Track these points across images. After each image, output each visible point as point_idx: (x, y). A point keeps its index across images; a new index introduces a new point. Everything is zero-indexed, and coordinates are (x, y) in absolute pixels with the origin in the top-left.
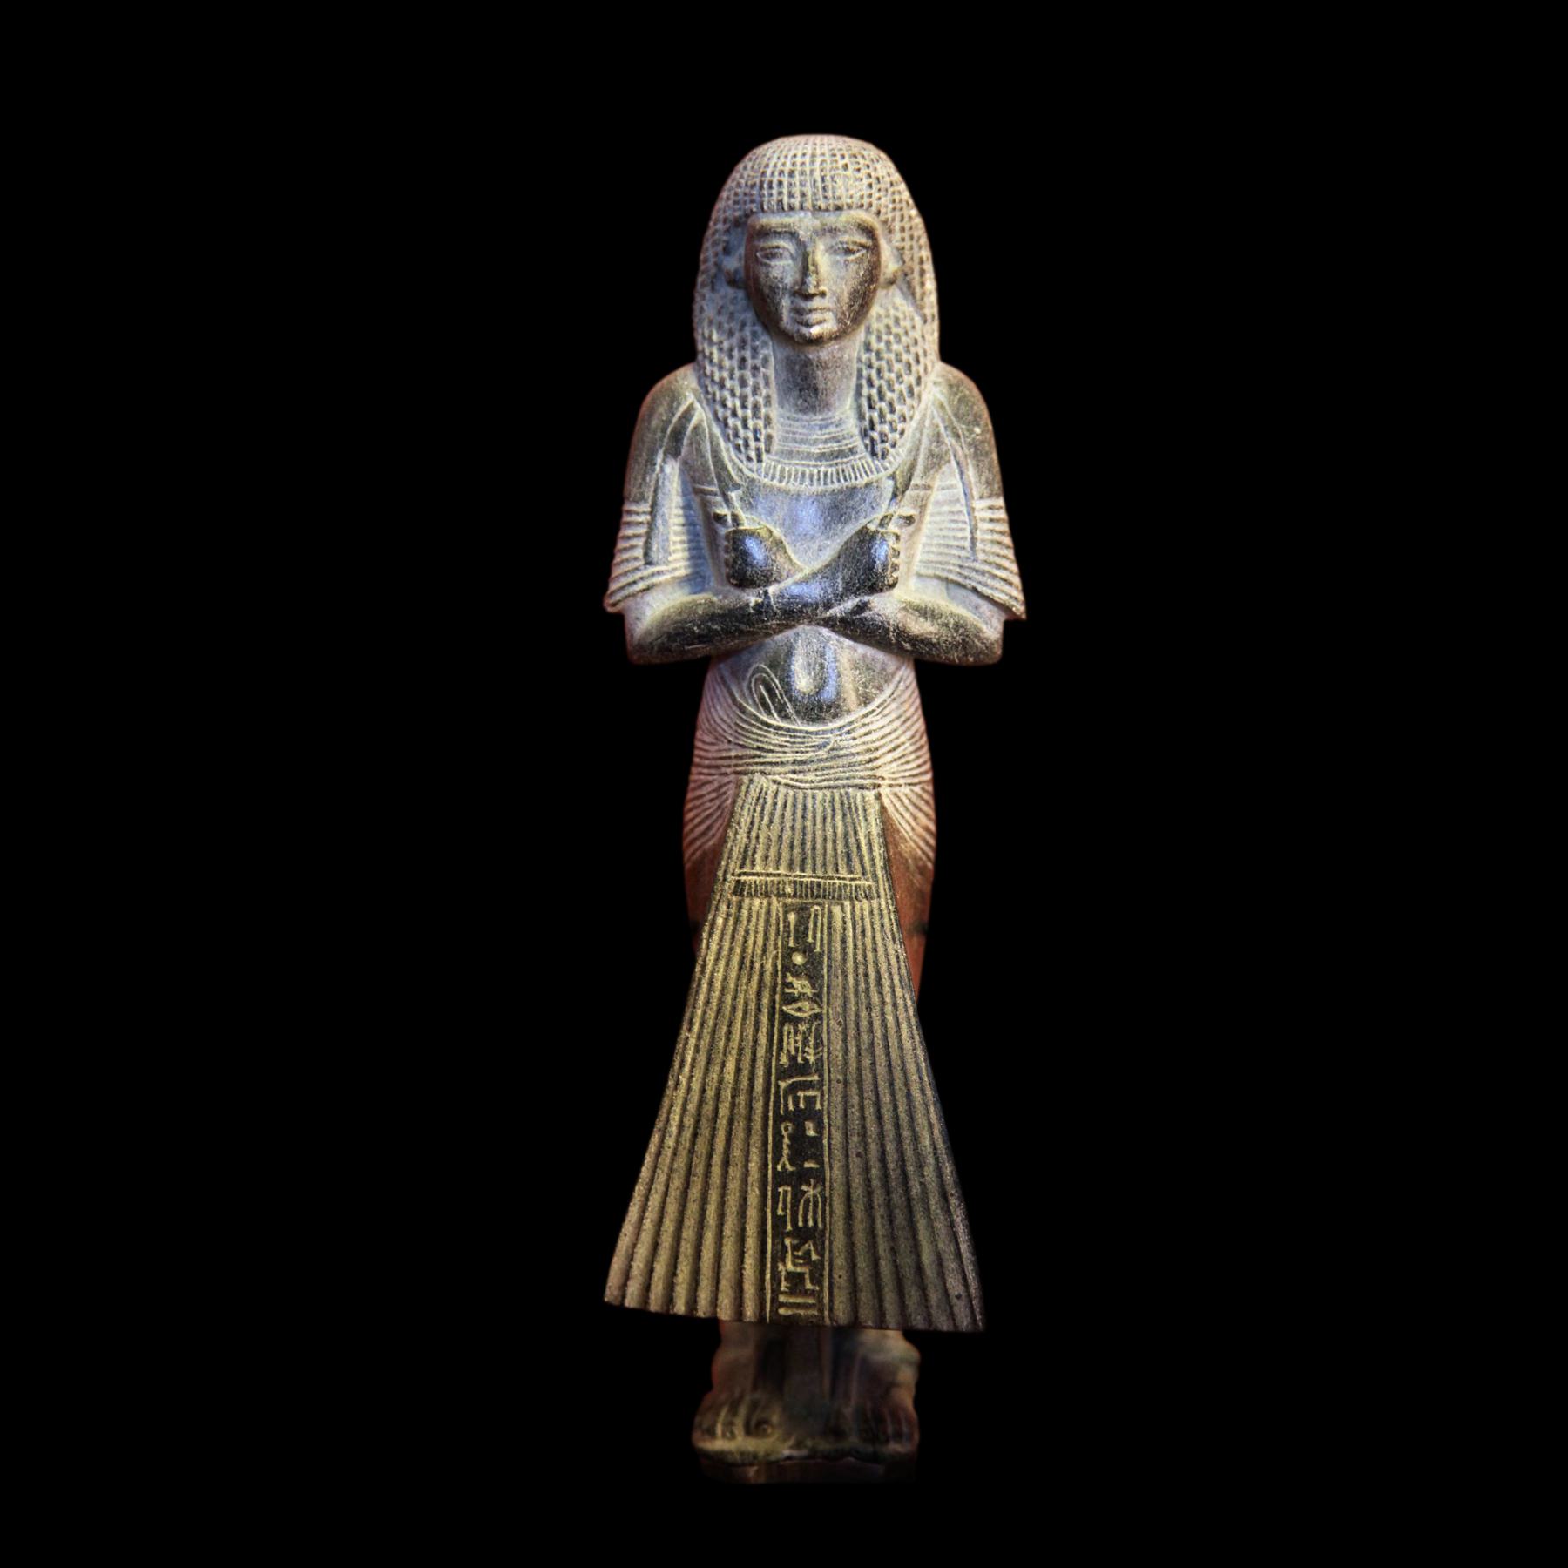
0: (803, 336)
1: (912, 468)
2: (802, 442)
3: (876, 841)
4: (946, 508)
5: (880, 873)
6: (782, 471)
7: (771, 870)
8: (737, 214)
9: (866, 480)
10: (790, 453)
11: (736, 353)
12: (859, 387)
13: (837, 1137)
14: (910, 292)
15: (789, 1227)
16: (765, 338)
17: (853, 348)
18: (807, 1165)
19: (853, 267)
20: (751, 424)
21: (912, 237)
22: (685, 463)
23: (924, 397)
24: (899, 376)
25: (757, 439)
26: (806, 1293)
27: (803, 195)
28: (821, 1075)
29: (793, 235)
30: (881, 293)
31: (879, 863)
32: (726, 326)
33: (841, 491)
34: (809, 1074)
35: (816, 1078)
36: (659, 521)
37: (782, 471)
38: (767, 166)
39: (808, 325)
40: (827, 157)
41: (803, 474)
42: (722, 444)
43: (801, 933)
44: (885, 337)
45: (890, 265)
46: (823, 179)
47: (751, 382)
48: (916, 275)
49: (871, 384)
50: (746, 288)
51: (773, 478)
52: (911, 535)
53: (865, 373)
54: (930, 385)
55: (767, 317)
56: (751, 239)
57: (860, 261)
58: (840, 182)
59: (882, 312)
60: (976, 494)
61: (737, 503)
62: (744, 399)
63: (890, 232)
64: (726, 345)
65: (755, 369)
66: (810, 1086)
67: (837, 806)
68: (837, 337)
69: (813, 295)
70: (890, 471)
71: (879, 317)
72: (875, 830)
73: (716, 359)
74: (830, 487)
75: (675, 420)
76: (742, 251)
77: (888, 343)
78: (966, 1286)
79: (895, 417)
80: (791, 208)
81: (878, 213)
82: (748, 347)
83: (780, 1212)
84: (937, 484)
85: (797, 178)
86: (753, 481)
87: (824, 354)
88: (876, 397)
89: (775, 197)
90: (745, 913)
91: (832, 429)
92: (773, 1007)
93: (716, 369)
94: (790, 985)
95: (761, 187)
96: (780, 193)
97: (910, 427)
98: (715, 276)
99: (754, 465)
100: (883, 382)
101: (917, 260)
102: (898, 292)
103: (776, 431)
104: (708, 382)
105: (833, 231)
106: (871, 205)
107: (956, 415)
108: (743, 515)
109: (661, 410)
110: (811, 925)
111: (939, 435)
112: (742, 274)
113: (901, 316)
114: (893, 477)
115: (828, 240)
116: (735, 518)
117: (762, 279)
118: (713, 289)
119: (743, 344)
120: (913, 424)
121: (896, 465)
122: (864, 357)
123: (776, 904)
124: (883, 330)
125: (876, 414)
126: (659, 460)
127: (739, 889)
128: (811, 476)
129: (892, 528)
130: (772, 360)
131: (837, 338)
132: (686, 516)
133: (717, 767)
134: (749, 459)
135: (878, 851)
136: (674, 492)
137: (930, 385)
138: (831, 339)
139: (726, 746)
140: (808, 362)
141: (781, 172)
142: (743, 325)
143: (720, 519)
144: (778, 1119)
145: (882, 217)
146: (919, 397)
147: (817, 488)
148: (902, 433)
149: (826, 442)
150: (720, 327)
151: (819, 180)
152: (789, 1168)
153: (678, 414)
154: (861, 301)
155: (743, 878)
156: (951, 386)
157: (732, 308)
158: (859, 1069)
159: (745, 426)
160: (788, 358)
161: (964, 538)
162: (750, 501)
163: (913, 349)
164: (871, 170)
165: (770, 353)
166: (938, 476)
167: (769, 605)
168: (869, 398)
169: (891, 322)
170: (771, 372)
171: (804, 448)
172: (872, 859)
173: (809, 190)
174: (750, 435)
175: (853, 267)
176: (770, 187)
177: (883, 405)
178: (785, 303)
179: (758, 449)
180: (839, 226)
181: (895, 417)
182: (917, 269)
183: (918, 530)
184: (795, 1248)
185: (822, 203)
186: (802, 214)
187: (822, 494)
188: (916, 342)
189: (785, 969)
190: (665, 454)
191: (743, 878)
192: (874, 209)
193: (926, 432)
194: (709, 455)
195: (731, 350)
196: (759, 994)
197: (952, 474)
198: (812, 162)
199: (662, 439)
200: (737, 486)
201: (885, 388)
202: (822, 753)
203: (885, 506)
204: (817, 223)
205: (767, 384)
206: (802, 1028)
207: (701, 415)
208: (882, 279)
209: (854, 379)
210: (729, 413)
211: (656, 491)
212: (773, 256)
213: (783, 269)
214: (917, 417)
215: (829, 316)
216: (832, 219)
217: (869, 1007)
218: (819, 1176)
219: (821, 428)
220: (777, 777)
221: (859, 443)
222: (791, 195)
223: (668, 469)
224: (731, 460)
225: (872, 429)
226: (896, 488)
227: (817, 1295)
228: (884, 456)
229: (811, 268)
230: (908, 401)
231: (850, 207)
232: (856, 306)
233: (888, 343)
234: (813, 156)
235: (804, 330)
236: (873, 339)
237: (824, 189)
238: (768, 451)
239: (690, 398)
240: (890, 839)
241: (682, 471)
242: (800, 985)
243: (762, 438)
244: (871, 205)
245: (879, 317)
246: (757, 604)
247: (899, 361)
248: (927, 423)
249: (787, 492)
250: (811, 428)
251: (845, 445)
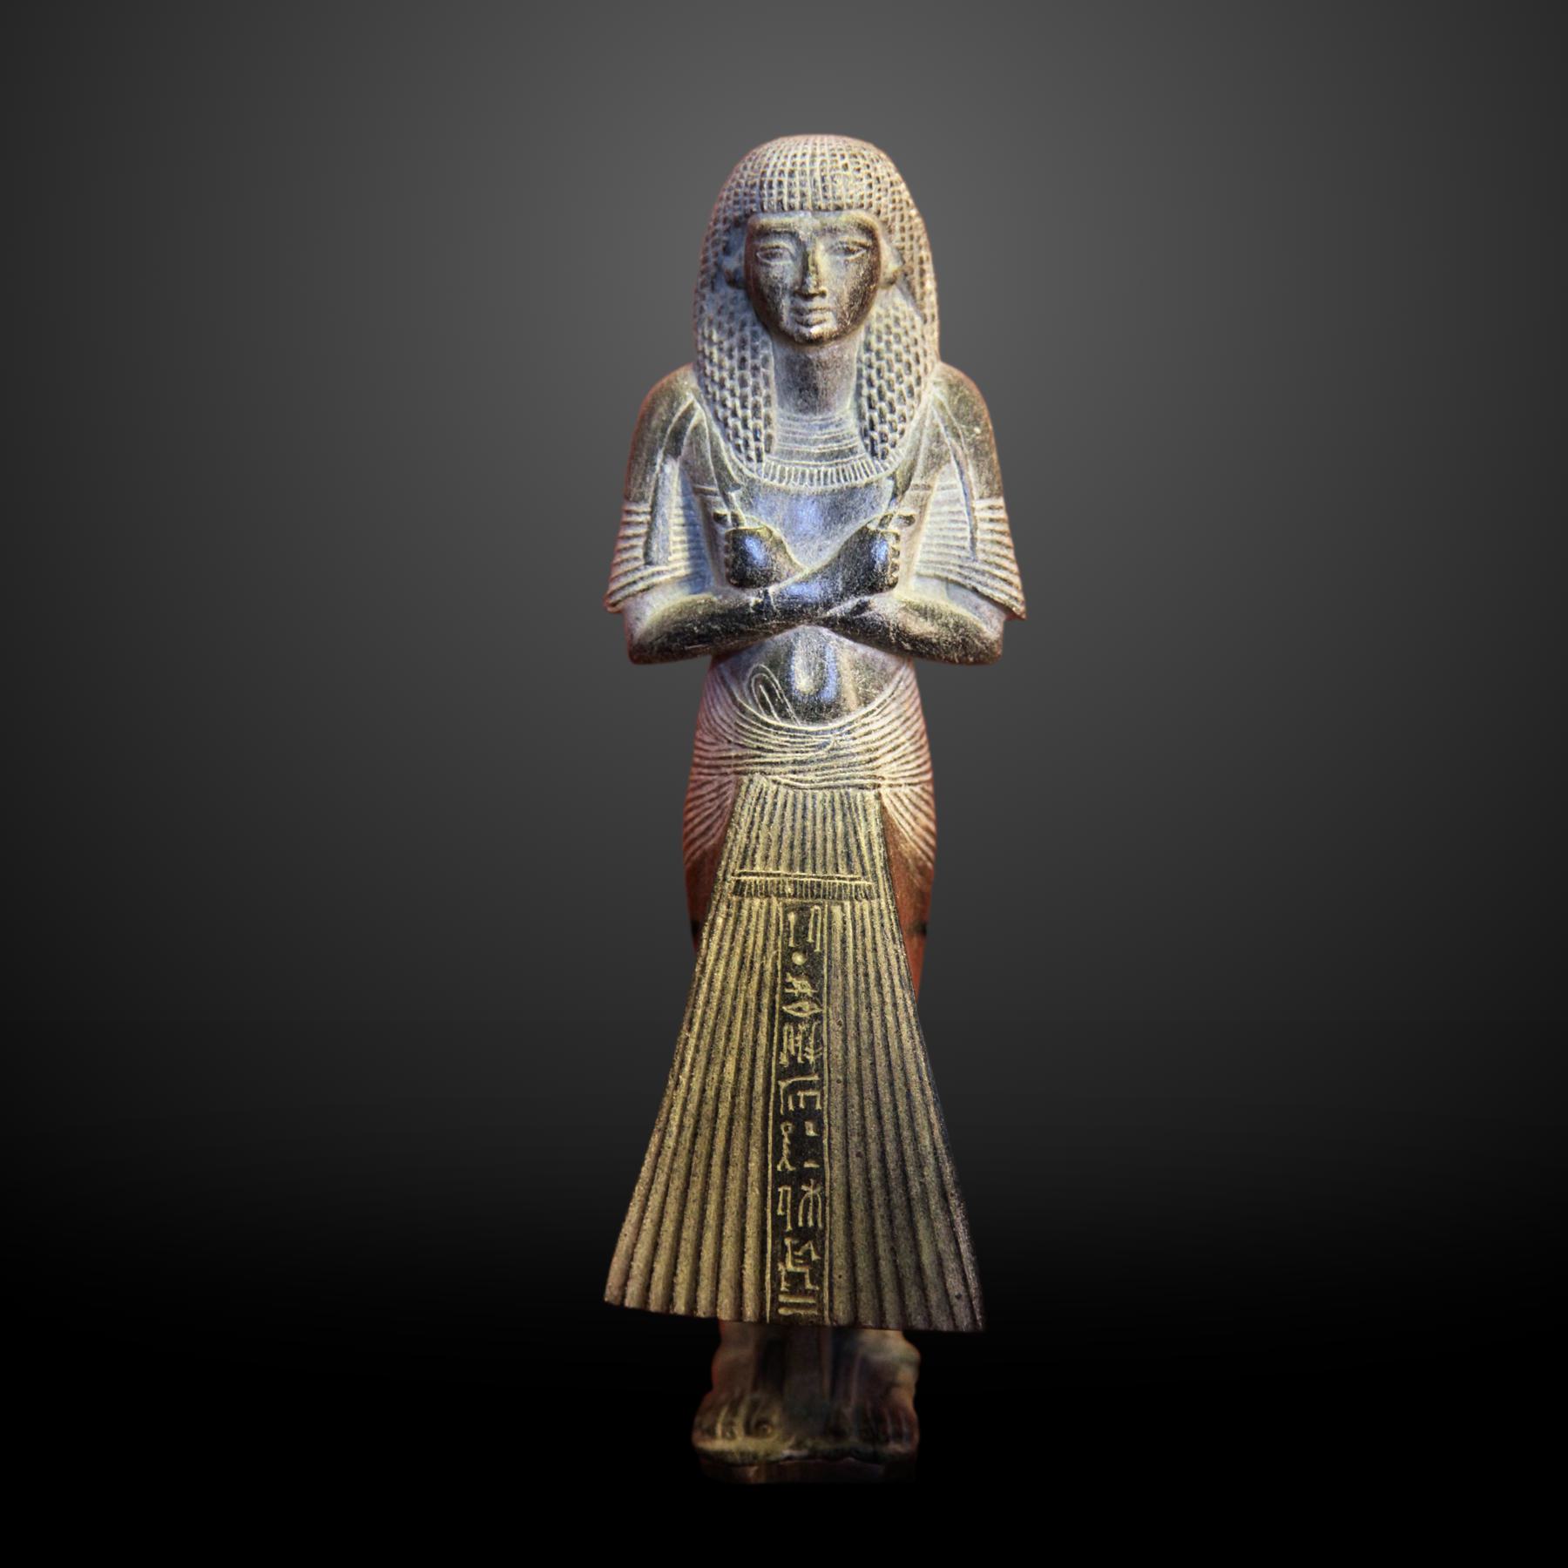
0: (803, 336)
1: (912, 468)
2: (802, 442)
3: (876, 841)
4: (946, 508)
5: (880, 873)
6: (782, 471)
7: (771, 870)
8: (737, 214)
9: (866, 480)
10: (790, 453)
11: (736, 353)
12: (859, 387)
13: (837, 1137)
14: (910, 292)
15: (789, 1227)
16: (765, 338)
17: (853, 348)
18: (807, 1165)
19: (853, 267)
20: (751, 424)
21: (912, 237)
22: (685, 463)
23: (924, 397)
24: (899, 376)
25: (757, 439)
26: (806, 1293)
27: (803, 195)
28: (821, 1075)
29: (793, 235)
30: (881, 293)
31: (879, 863)
32: (726, 326)
33: (841, 491)
34: (809, 1074)
35: (816, 1078)
36: (659, 521)
37: (782, 471)
38: (767, 166)
39: (808, 325)
40: (827, 157)
41: (803, 474)
42: (722, 444)
43: (801, 933)
44: (885, 337)
45: (890, 265)
46: (823, 179)
47: (751, 382)
48: (916, 275)
49: (871, 384)
50: (746, 288)
51: (773, 478)
52: (911, 535)
53: (865, 373)
54: (930, 385)
55: (767, 317)
56: (751, 239)
57: (860, 261)
58: (840, 182)
59: (882, 312)
60: (976, 494)
61: (737, 503)
62: (744, 399)
63: (890, 232)
64: (726, 345)
65: (755, 369)
66: (810, 1086)
67: (837, 806)
68: (837, 337)
69: (813, 295)
70: (890, 471)
71: (879, 317)
72: (875, 830)
73: (716, 359)
74: (830, 487)
75: (675, 420)
76: (742, 251)
77: (888, 343)
78: (966, 1286)
79: (895, 417)
80: (791, 208)
81: (878, 213)
82: (748, 347)
83: (780, 1212)
84: (937, 484)
85: (797, 178)
86: (753, 481)
87: (824, 354)
88: (876, 397)
89: (775, 197)
90: (745, 913)
91: (832, 429)
92: (773, 1007)
93: (716, 369)
94: (790, 985)
95: (761, 187)
96: (780, 193)
97: (910, 427)
98: (715, 276)
99: (754, 465)
100: (883, 382)
101: (917, 260)
102: (898, 292)
103: (776, 431)
104: (708, 382)
105: (833, 231)
106: (871, 205)
107: (956, 415)
108: (743, 515)
109: (661, 410)
110: (811, 925)
111: (939, 435)
112: (742, 274)
113: (901, 316)
114: (893, 477)
115: (828, 240)
116: (735, 518)
117: (762, 279)
118: (713, 289)
119: (743, 344)
120: (913, 424)
121: (896, 465)
122: (864, 357)
123: (776, 904)
124: (883, 330)
125: (876, 414)
126: (659, 460)
127: (739, 889)
128: (811, 476)
129: (892, 528)
130: (772, 360)
131: (837, 338)
132: (686, 516)
133: (717, 767)
134: (749, 459)
135: (878, 851)
136: (674, 492)
137: (930, 385)
138: (831, 339)
139: (726, 746)
140: (808, 362)
141: (781, 172)
142: (743, 325)
143: (720, 519)
144: (778, 1119)
145: (882, 217)
146: (919, 397)
147: (817, 488)
148: (902, 433)
149: (826, 442)
150: (720, 327)
151: (819, 180)
152: (789, 1168)
153: (678, 414)
154: (861, 301)
155: (743, 878)
156: (951, 386)
157: (732, 308)
158: (859, 1069)
159: (745, 426)
160: (788, 358)
161: (964, 538)
162: (750, 501)
163: (913, 349)
164: (871, 170)
165: (770, 353)
166: (938, 476)
167: (769, 605)
168: (869, 398)
169: (891, 322)
170: (771, 372)
171: (804, 448)
172: (872, 859)
173: (809, 190)
174: (750, 435)
175: (853, 267)
176: (770, 187)
177: (883, 405)
178: (785, 303)
179: (758, 449)
180: (839, 226)
181: (895, 417)
182: (917, 269)
183: (918, 530)
184: (795, 1248)
185: (822, 203)
186: (802, 214)
187: (822, 494)
188: (916, 342)
189: (785, 969)
190: (665, 454)
191: (743, 878)
192: (874, 209)
193: (926, 432)
194: (709, 455)
195: (731, 350)
196: (759, 994)
197: (952, 474)
198: (812, 162)
199: (662, 439)
200: (737, 486)
201: (885, 388)
202: (822, 753)
203: (885, 506)
204: (817, 223)
205: (767, 384)
206: (802, 1028)
207: (701, 415)
208: (882, 279)
209: (854, 379)
210: (729, 413)
211: (656, 491)
212: (773, 256)
213: (783, 269)
214: (917, 417)
215: (829, 316)
216: (832, 219)
217: (869, 1007)
218: (819, 1176)
219: (821, 428)
220: (777, 777)
221: (859, 443)
222: (791, 195)
223: (668, 469)
224: (731, 460)
225: (872, 429)
226: (896, 488)
227: (817, 1295)
228: (884, 456)
229: (811, 268)
230: (908, 401)
231: (850, 207)
232: (856, 306)
233: (888, 343)
234: (813, 156)
235: (804, 330)
236: (873, 339)
237: (824, 189)
238: (768, 451)
239: (690, 398)
240: (890, 839)
241: (682, 471)
242: (800, 985)
243: (762, 438)
244: (871, 205)
245: (879, 317)
246: (757, 604)
247: (899, 361)
248: (927, 423)
249: (787, 492)
250: (811, 428)
251: (845, 445)
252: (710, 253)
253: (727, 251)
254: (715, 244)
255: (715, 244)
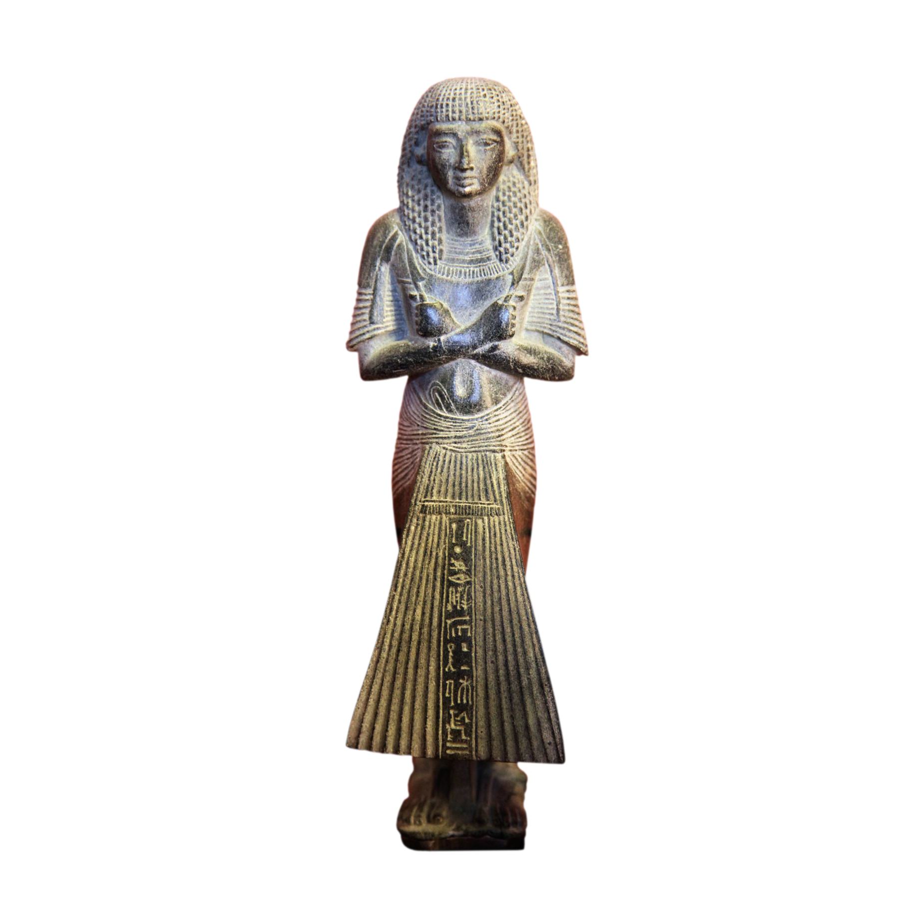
0: (460, 193)
1: (523, 268)
2: (460, 253)
3: (502, 482)
4: (542, 292)
5: (504, 501)
6: (449, 270)
7: (442, 499)
8: (423, 123)
9: (496, 275)
10: (453, 260)
11: (422, 202)
12: (493, 222)
13: (480, 652)
14: (522, 167)
15: (453, 704)
16: (439, 194)
17: (489, 200)
18: (463, 668)
19: (489, 153)
20: (430, 243)
21: (523, 136)
22: (393, 265)
23: (530, 228)
24: (516, 216)
25: (434, 252)
26: (462, 741)
27: (460, 112)
28: (471, 617)
29: (455, 135)
30: (505, 168)
31: (504, 495)
32: (416, 187)
33: (482, 282)
34: (464, 616)
35: (468, 618)
36: (378, 299)
37: (449, 270)
38: (440, 95)
39: (463, 186)
40: (474, 90)
41: (461, 272)
42: (414, 254)
43: (459, 535)
44: (507, 193)
45: (510, 152)
46: (472, 103)
47: (430, 219)
48: (525, 158)
49: (499, 220)
50: (428, 165)
51: (443, 274)
52: (522, 307)
53: (496, 214)
54: (533, 221)
55: (440, 182)
56: (430, 137)
57: (493, 150)
58: (481, 104)
59: (506, 179)
60: (559, 283)
61: (422, 289)
62: (426, 229)
63: (510, 133)
64: (416, 198)
65: (433, 211)
66: (465, 622)
67: (480, 462)
68: (480, 193)
69: (466, 169)
70: (510, 270)
71: (504, 182)
72: (502, 476)
73: (410, 206)
74: (476, 279)
75: (387, 241)
76: (425, 144)
77: (509, 197)
79: (513, 239)
80: (454, 119)
81: (504, 122)
82: (429, 199)
83: (447, 695)
84: (537, 278)
85: (457, 102)
86: (432, 276)
87: (473, 203)
88: (502, 228)
89: (444, 113)
90: (427, 523)
91: (477, 246)
92: (443, 578)
93: (410, 212)
94: (453, 565)
95: (437, 107)
96: (447, 111)
97: (522, 245)
98: (410, 158)
99: (432, 266)
100: (506, 219)
101: (525, 149)
102: (515, 167)
103: (445, 247)
104: (406, 219)
105: (478, 133)
106: (499, 118)
107: (548, 238)
108: (426, 295)
109: (379, 235)
110: (465, 531)
111: (538, 249)
112: (426, 157)
113: (516, 181)
114: (512, 273)
115: (475, 137)
116: (422, 297)
117: (437, 160)
118: (409, 166)
119: (426, 197)
120: (524, 243)
121: (514, 267)
122: (496, 205)
123: (445, 518)
124: (506, 189)
125: (502, 238)
126: (378, 264)
127: (424, 510)
128: (465, 273)
129: (512, 303)
130: (443, 206)
131: (480, 194)
132: (393, 296)
133: (411, 440)
134: (430, 263)
135: (503, 488)
136: (386, 282)
137: (533, 221)
138: (476, 194)
139: (416, 428)
140: (463, 208)
141: (448, 99)
142: (426, 186)
143: (413, 297)
144: (446, 642)
145: (506, 125)
146: (527, 227)
147: (469, 280)
148: (517, 248)
149: (473, 253)
150: (413, 187)
151: (469, 103)
152: (453, 670)
153: (389, 237)
154: (494, 173)
155: (426, 504)
156: (545, 221)
157: (419, 177)
158: (492, 613)
159: (427, 244)
160: (452, 205)
161: (552, 309)
162: (430, 287)
163: (523, 200)
164: (499, 98)
165: (441, 202)
166: (538, 273)
167: (441, 347)
168: (498, 228)
169: (511, 185)
170: (442, 213)
171: (461, 257)
172: (500, 493)
173: (464, 109)
174: (430, 249)
175: (489, 153)
176: (442, 107)
177: (507, 232)
178: (450, 174)
179: (434, 258)
180: (481, 129)
181: (513, 239)
182: (526, 154)
183: (526, 304)
184: (456, 715)
185: (471, 117)
186: (460, 123)
187: (472, 284)
188: (525, 196)
189: (450, 555)
190: (381, 260)
191: (426, 504)
192: (501, 120)
193: (531, 247)
194: (406, 261)
195: (419, 201)
196: (435, 570)
197: (546, 272)
198: (466, 93)
199: (379, 252)
200: (422, 279)
201: (507, 222)
202: (471, 432)
203: (507, 290)
204: (468, 128)
205: (440, 220)
206: (460, 589)
207: (402, 238)
208: (506, 160)
209: (490, 217)
210: (418, 237)
211: (376, 282)
212: (443, 147)
213: (449, 154)
214: (526, 239)
215: (475, 181)
216: (477, 126)
217: (498, 577)
218: (469, 674)
219: (471, 245)
220: (445, 446)
221: (492, 254)
222: (453, 112)
223: (383, 269)
224: (419, 264)
225: (500, 246)
226: (514, 280)
227: (468, 742)
228: (507, 261)
229: (465, 154)
230: (521, 230)
231: (487, 119)
232: (491, 176)
233: (509, 197)
234: (466, 89)
235: (461, 189)
236: (501, 194)
237: (473, 108)
238: (440, 259)
239: (396, 228)
240: (510, 481)
241: (391, 270)
242: (459, 565)
243: (437, 251)
244: (499, 118)
245: (504, 182)
246: (434, 346)
247: (516, 207)
248: (532, 242)
249: (451, 282)
250: (465, 245)
251: (485, 255)
252: (407, 145)
253: (417, 144)
254: (410, 140)
255: (410, 140)
